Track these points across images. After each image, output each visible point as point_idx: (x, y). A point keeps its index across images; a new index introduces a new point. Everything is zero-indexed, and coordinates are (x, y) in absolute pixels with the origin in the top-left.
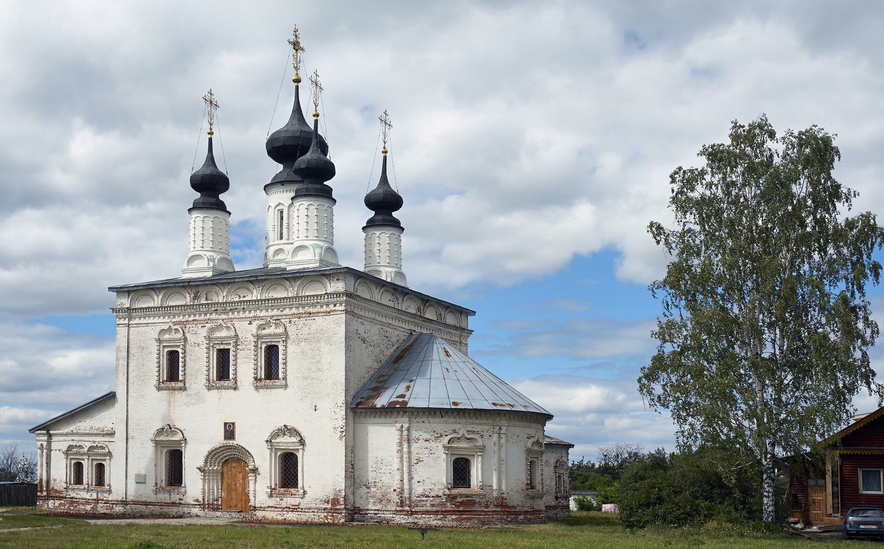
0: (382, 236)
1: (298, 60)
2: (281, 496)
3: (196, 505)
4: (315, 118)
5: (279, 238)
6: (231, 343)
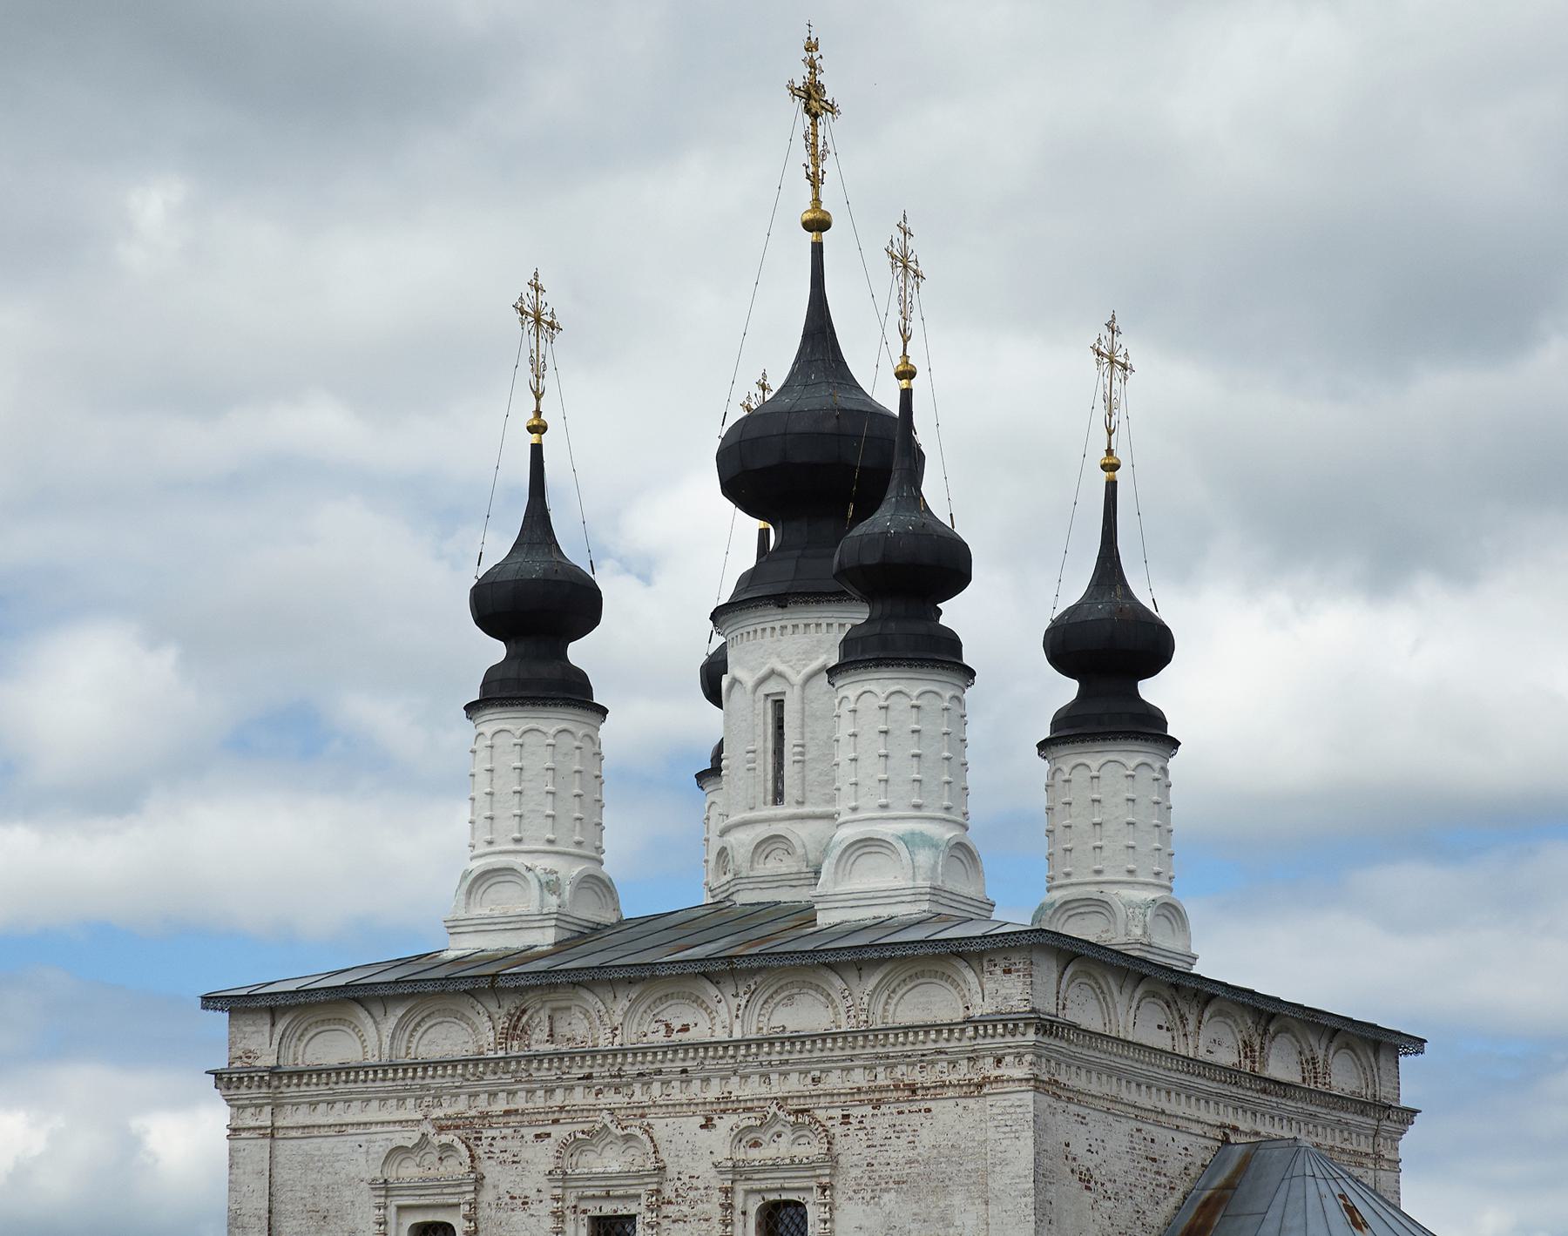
1: (820, 148)
4: (904, 383)
5: (770, 798)
6: (639, 1196)
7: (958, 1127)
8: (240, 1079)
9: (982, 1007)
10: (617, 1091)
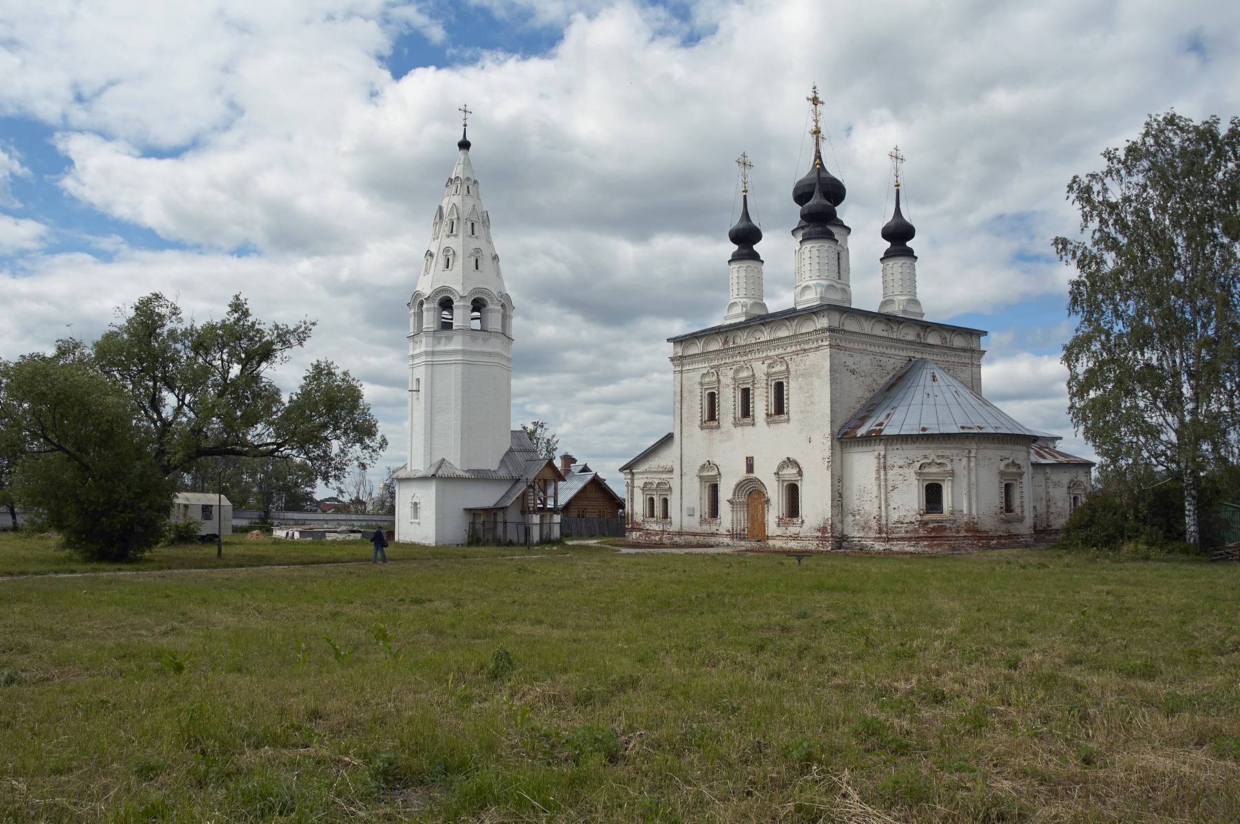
0: (897, 264)
2: (786, 525)
9: (819, 327)
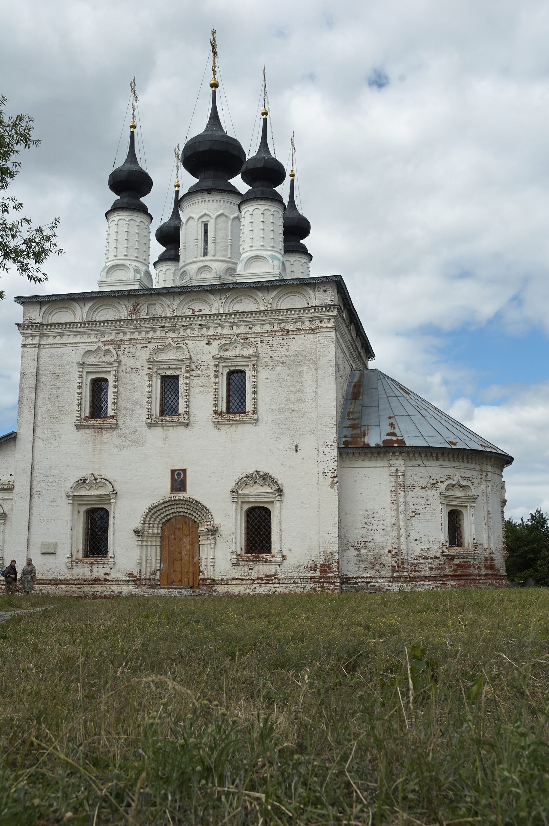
3: (129, 581)
5: (202, 254)
6: (181, 368)
7: (305, 344)
8: (28, 326)
9: (314, 303)
10: (174, 332)
